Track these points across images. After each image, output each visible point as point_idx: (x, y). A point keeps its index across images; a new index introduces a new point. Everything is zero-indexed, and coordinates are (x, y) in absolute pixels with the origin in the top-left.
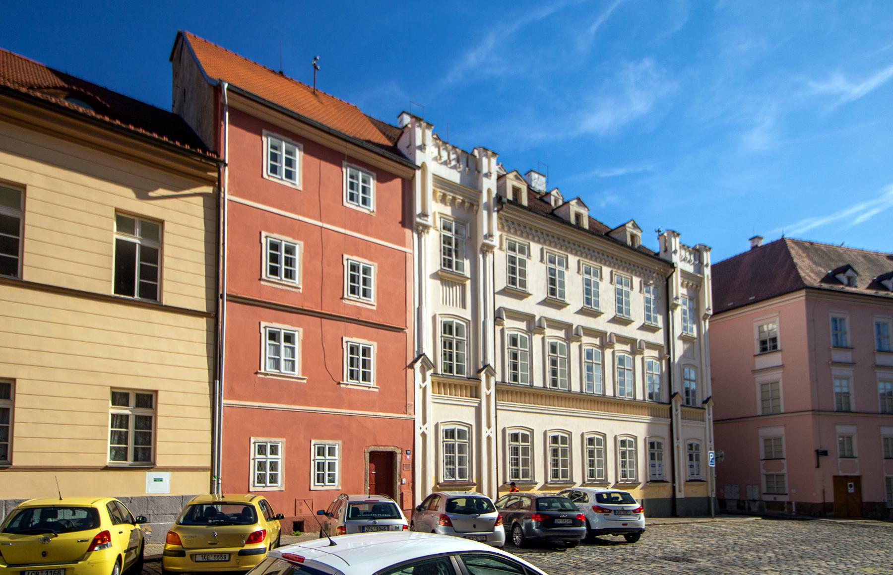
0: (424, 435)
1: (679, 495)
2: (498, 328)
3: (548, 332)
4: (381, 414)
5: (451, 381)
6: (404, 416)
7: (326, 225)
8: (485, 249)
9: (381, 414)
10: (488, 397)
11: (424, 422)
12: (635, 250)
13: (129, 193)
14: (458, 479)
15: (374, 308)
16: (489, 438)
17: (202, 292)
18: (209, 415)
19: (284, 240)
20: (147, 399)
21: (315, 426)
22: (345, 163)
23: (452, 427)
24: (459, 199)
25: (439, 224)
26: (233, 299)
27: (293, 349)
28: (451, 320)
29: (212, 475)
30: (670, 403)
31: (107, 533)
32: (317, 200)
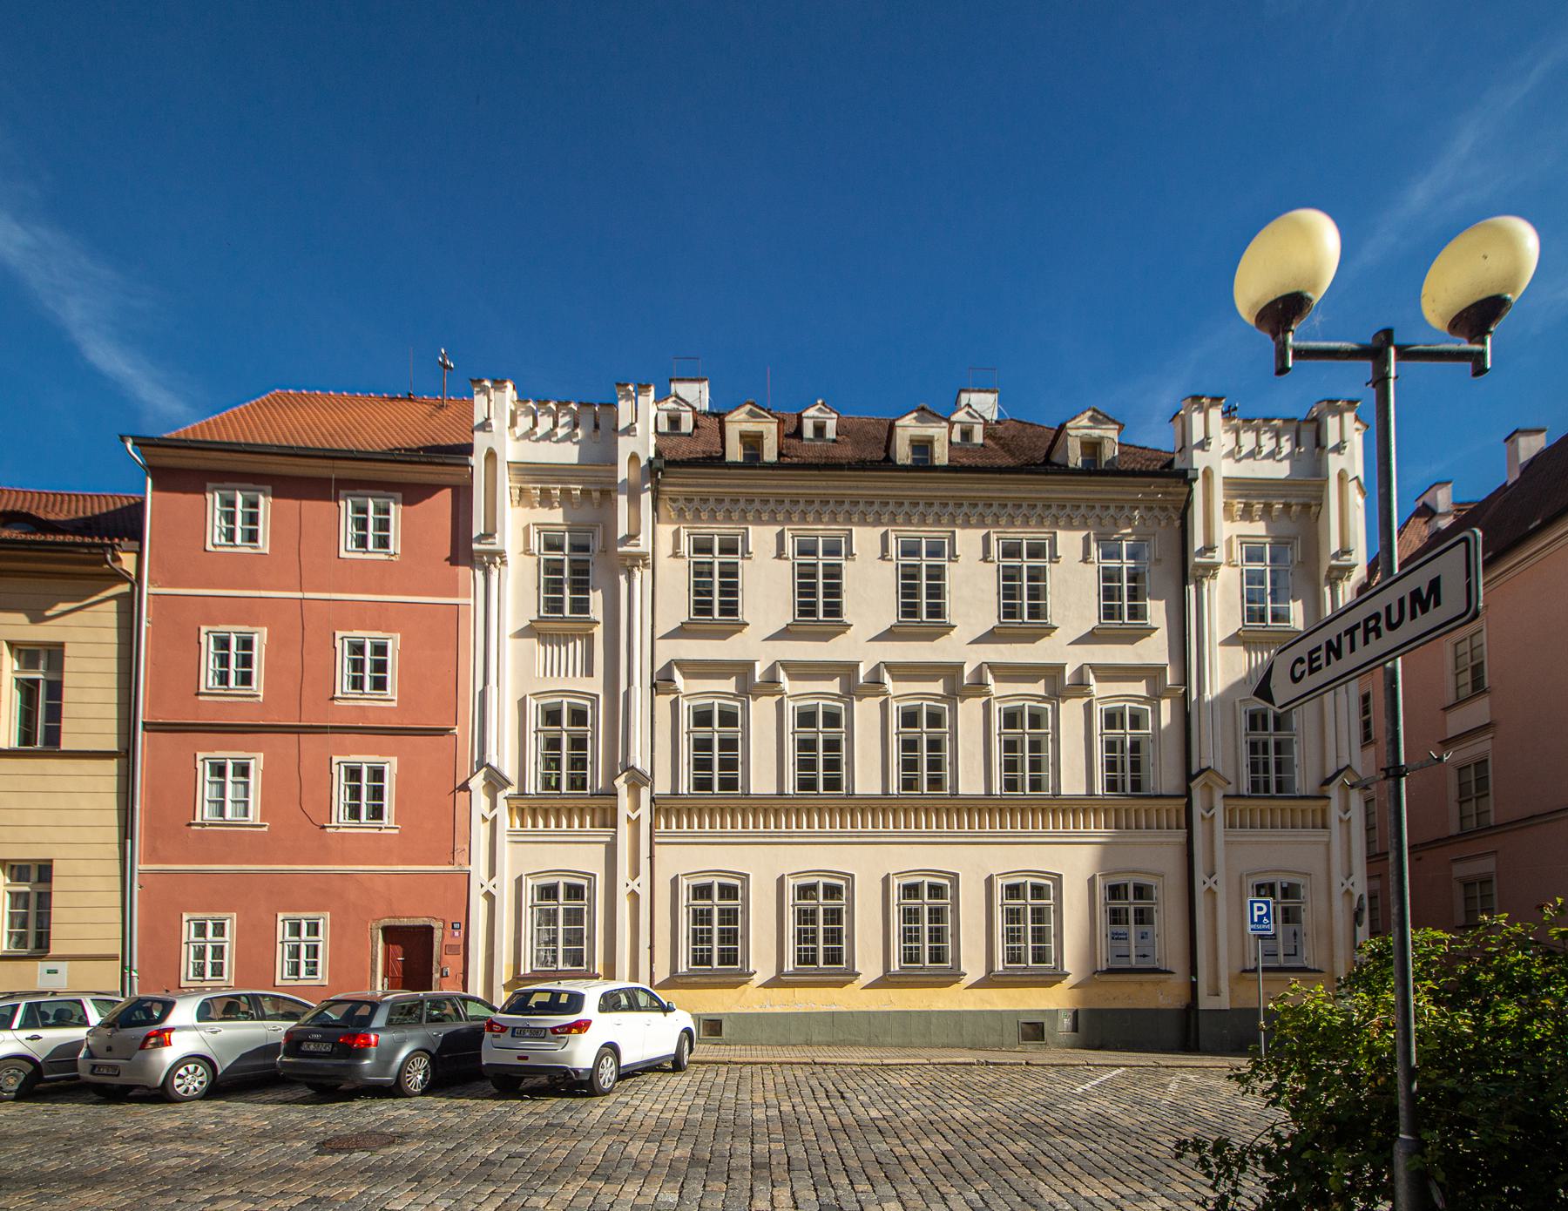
0: (634, 896)
1: (1206, 1002)
2: (663, 702)
3: (1096, 688)
4: (400, 868)
5: (557, 803)
6: (449, 868)
7: (308, 595)
8: (1335, 574)
9: (400, 868)
10: (635, 824)
11: (492, 874)
12: (1114, 472)
13: (21, 618)
14: (560, 967)
15: (394, 704)
16: (634, 896)
17: (112, 726)
18: (119, 888)
19: (369, 637)
20: (45, 871)
21: (282, 892)
22: (209, 485)
23: (552, 880)
24: (576, 490)
25: (1238, 554)
26: (150, 727)
27: (246, 785)
28: (710, 701)
29: (124, 967)
30: (1188, 794)
31: (588, 1023)
32: (301, 559)
